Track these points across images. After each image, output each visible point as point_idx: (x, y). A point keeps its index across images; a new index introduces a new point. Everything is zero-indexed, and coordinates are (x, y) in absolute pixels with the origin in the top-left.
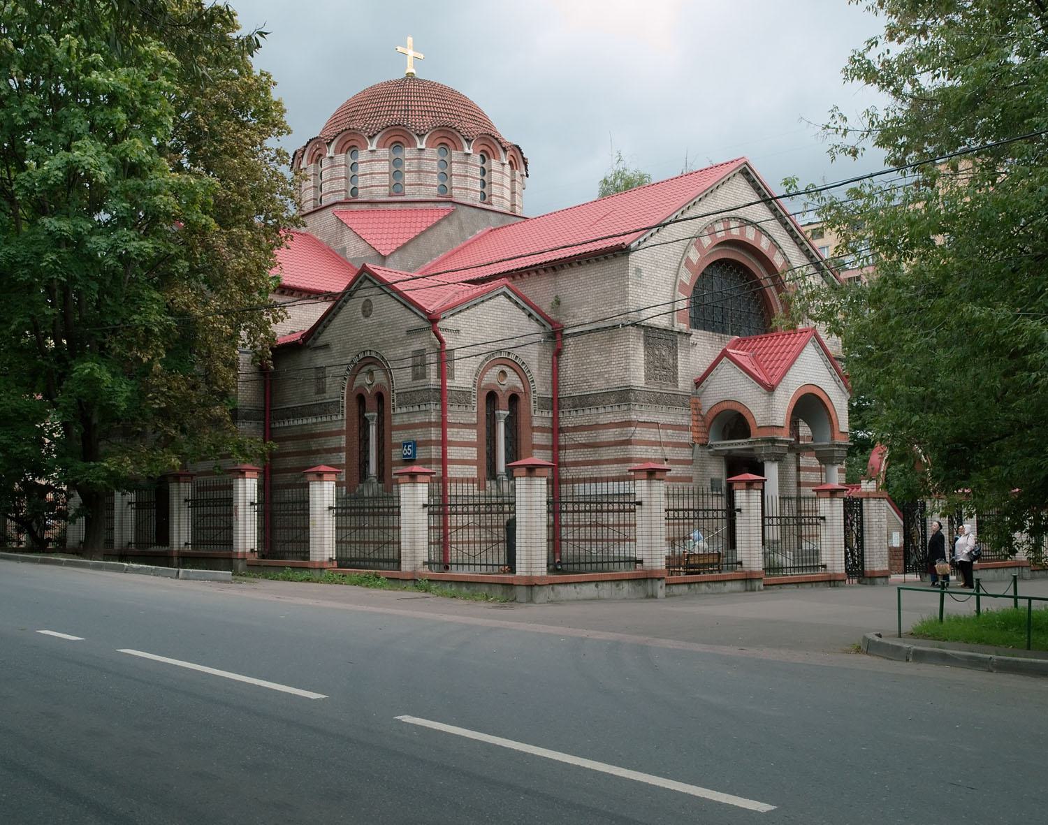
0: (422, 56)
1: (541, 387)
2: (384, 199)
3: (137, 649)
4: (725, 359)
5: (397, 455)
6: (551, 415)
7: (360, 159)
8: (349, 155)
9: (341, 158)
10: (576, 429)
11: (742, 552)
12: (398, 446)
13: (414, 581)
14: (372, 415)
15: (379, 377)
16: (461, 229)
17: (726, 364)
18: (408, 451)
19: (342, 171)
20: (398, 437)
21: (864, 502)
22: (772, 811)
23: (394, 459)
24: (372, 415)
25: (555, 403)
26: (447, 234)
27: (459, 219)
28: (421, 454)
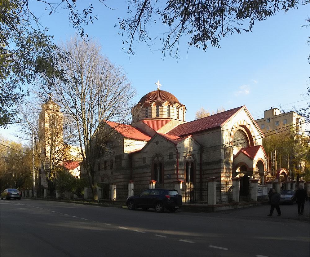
0: (161, 85)
1: (198, 160)
2: (154, 118)
3: (168, 230)
4: (241, 153)
5: (165, 177)
6: (200, 167)
7: (149, 109)
8: (146, 108)
9: (144, 109)
10: (206, 170)
11: (46, 190)
12: (166, 175)
13: (186, 208)
14: (158, 168)
15: (160, 158)
16: (173, 124)
17: (241, 154)
18: (168, 176)
19: (144, 112)
20: (166, 173)
21: (276, 184)
22: (257, 255)
23: (165, 178)
24: (158, 168)
25: (201, 164)
26: (170, 126)
27: (172, 122)
28: (172, 176)
